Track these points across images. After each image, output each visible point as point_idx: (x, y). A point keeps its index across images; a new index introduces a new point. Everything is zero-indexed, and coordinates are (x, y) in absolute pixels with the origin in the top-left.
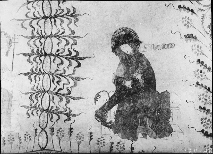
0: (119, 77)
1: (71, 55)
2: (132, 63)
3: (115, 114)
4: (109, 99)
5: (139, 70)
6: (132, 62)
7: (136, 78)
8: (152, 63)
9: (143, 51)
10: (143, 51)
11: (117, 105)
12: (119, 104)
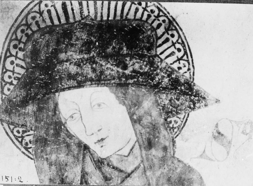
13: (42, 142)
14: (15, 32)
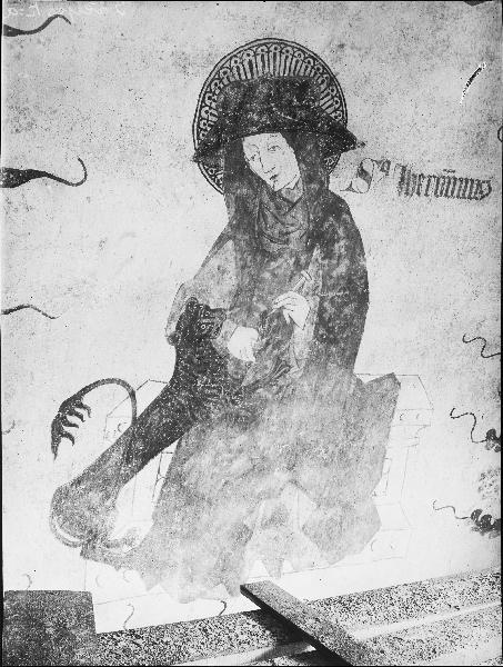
0: (207, 308)
1: (289, 328)
2: (287, 242)
3: (157, 495)
4: (134, 419)
5: (309, 278)
6: (288, 233)
7: (285, 313)
8: (373, 252)
9: (347, 189)
10: (347, 189)
11: (172, 447)
12: (179, 446)
13: (228, 178)
14: (210, 85)
